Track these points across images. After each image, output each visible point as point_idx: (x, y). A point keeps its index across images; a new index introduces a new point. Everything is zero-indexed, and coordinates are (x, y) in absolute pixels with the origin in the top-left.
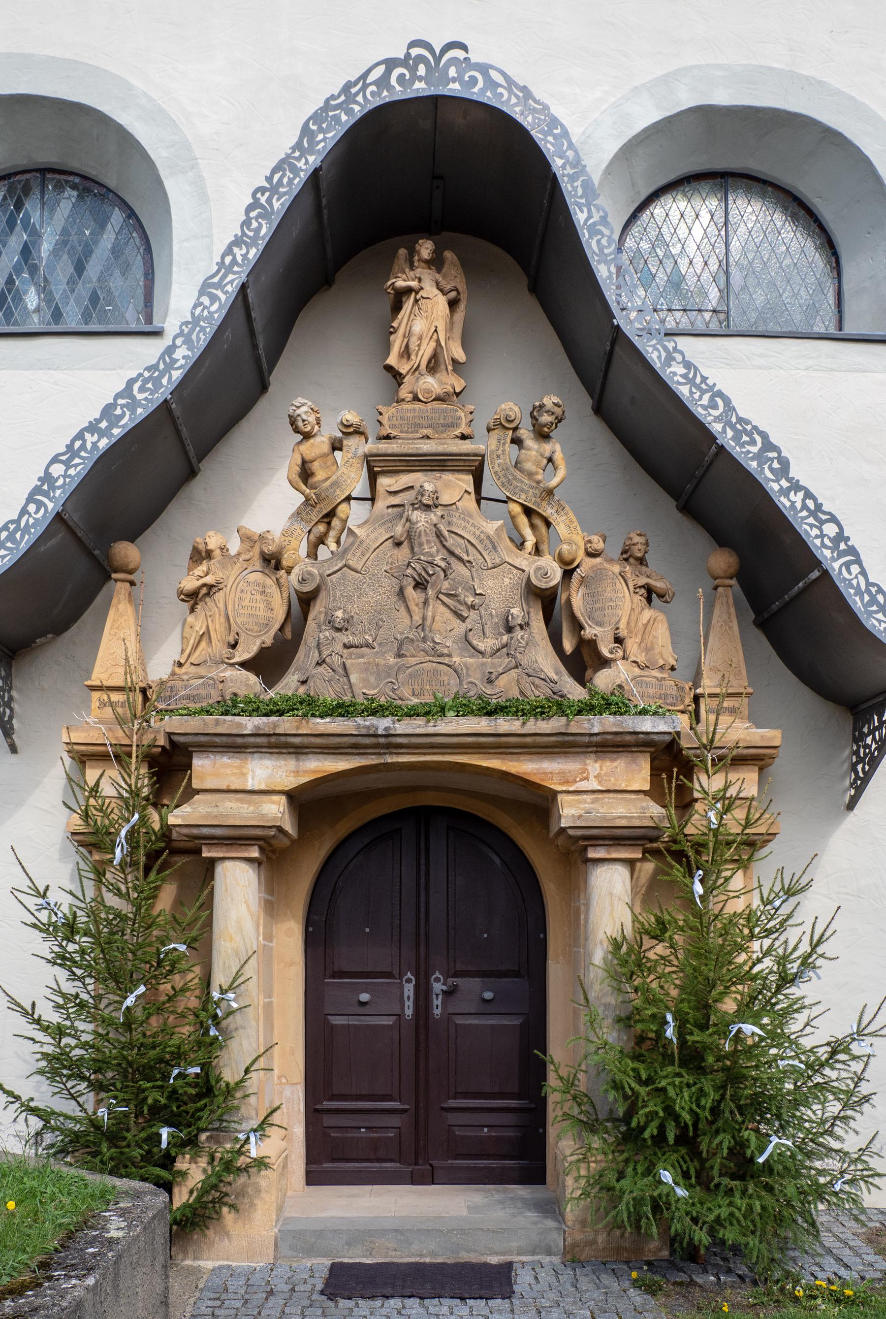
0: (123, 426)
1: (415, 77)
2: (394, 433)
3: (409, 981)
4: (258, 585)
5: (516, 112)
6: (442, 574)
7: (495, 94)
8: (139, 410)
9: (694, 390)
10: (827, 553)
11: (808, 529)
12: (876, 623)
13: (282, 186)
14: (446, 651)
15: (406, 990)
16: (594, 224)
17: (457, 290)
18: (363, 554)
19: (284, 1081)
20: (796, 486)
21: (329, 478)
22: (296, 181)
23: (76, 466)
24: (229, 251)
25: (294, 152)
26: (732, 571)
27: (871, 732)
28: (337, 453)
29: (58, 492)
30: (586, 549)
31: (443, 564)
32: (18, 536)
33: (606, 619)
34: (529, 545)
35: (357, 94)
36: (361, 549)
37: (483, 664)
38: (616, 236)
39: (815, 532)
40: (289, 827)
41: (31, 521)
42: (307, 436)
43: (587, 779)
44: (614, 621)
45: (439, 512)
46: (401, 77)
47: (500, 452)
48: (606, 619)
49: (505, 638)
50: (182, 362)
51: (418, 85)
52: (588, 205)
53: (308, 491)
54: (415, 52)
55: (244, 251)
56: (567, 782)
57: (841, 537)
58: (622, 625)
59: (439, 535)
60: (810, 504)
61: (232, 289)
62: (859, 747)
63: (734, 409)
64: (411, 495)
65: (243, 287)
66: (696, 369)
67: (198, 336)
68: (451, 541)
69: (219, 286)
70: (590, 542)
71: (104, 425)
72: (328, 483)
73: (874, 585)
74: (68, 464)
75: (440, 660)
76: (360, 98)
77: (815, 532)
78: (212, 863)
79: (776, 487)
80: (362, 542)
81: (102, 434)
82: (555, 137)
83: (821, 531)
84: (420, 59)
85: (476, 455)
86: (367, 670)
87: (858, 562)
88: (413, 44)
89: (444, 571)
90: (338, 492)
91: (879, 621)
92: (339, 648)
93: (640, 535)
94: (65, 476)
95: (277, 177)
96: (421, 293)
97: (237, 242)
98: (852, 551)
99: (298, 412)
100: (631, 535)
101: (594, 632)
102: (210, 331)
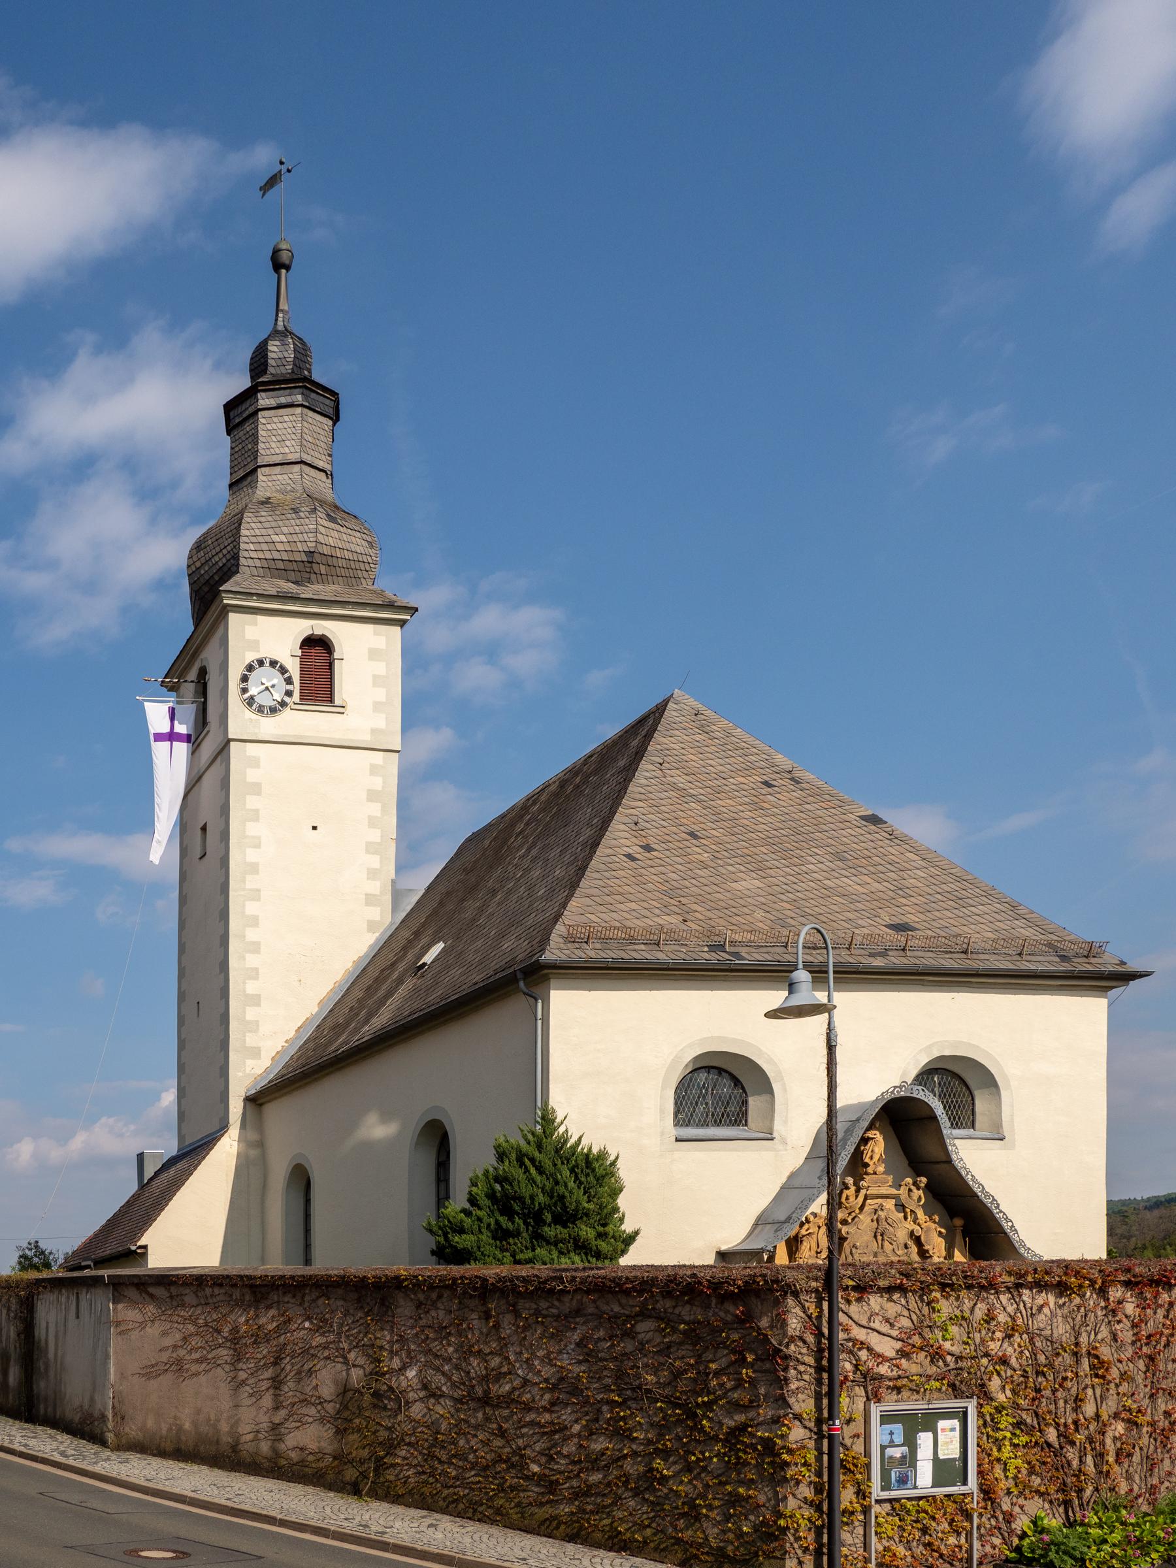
11: (1004, 1224)
20: (1001, 1212)
57: (1013, 1226)
98: (1016, 1230)
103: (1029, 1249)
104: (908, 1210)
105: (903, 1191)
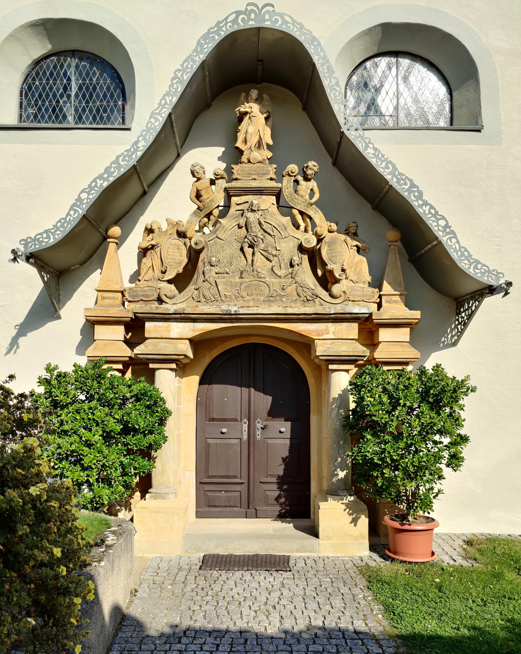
0: (114, 177)
1: (250, 19)
2: (239, 177)
3: (245, 423)
4: (176, 245)
5: (297, 35)
6: (261, 241)
7: (287, 26)
8: (122, 170)
9: (378, 160)
10: (441, 233)
11: (432, 223)
12: (464, 265)
13: (188, 68)
14: (263, 276)
15: (244, 427)
16: (333, 85)
17: (269, 112)
18: (225, 232)
19: (186, 469)
20: (426, 204)
21: (209, 198)
22: (194, 67)
23: (93, 194)
24: (163, 98)
25: (193, 53)
26: (397, 238)
27: (464, 311)
28: (212, 186)
29: (84, 206)
30: (328, 229)
31: (262, 237)
32: (65, 225)
33: (337, 261)
34: (302, 227)
35: (223, 27)
36: (224, 230)
37: (280, 282)
38: (343, 91)
39: (435, 224)
40: (191, 355)
41: (72, 218)
42: (199, 179)
43: (328, 333)
44: (341, 262)
45: (260, 213)
46: (243, 19)
47: (288, 186)
48: (337, 261)
49: (290, 270)
50: (142, 148)
51: (251, 23)
52: (330, 77)
53: (199, 203)
54: (249, 8)
55: (170, 98)
56: (319, 335)
57: (447, 226)
58: (345, 264)
59: (260, 224)
60: (433, 211)
61: (165, 115)
62: (459, 317)
63: (397, 169)
64: (247, 205)
65: (170, 114)
66: (379, 151)
67: (149, 136)
68: (265, 226)
69: (159, 114)
70: (330, 226)
71: (105, 176)
72: (209, 200)
73: (463, 247)
74: (89, 193)
75: (260, 280)
76: (224, 29)
77: (435, 224)
78: (154, 370)
79: (416, 204)
80: (224, 227)
81: (105, 180)
82: (315, 46)
83: (438, 223)
84: (252, 11)
85: (277, 188)
86: (226, 284)
87: (455, 237)
88: (249, 4)
89: (262, 240)
90: (213, 204)
91: (466, 264)
92: (213, 274)
93: (354, 223)
94: (87, 199)
95: (185, 64)
96: (252, 114)
97: (167, 94)
98: (453, 232)
99: (195, 168)
100: (350, 223)
101: (332, 267)
102: (155, 134)
103: (477, 262)
104: (295, 212)
105: (287, 184)
